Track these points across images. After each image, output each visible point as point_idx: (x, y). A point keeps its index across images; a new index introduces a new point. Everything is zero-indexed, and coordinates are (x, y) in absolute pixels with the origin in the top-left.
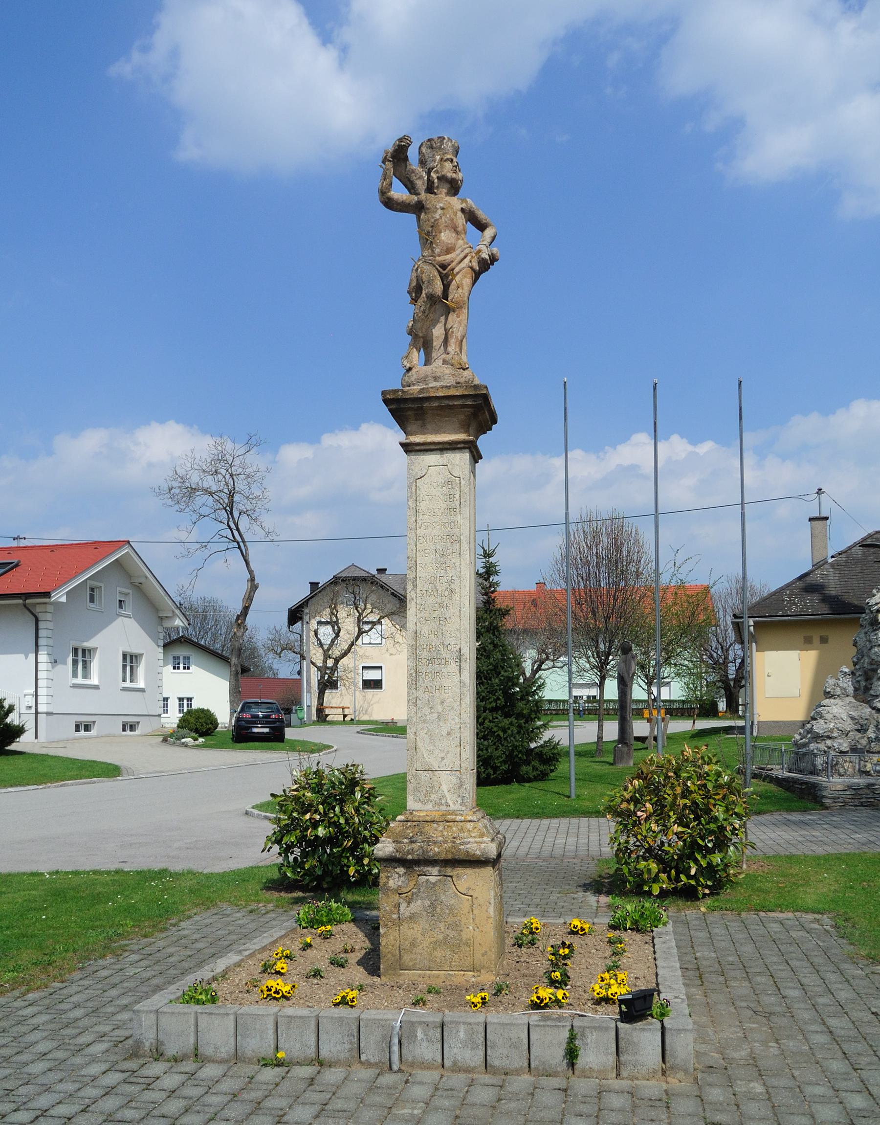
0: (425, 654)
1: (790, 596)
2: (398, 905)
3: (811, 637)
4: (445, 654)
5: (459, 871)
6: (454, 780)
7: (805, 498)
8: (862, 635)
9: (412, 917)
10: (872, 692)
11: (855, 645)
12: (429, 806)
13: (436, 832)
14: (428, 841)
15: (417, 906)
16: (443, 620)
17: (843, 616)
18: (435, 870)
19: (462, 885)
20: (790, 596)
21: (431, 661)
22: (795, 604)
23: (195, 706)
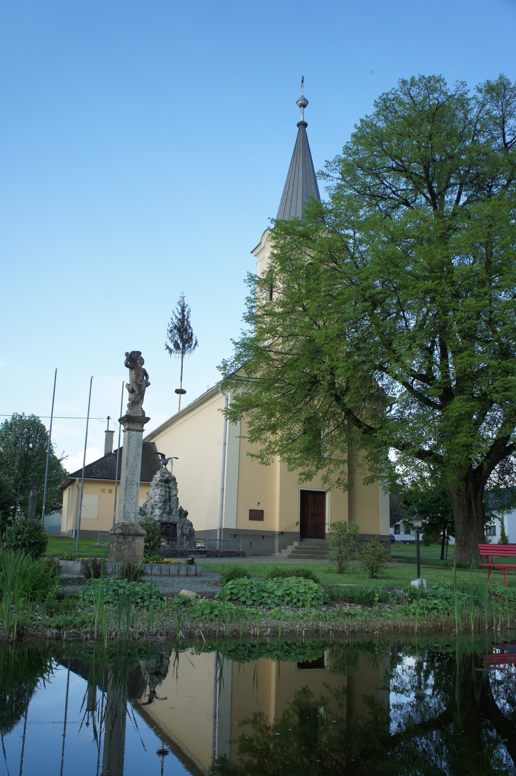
0: (129, 482)
1: (96, 468)
2: (121, 546)
3: (105, 490)
4: (134, 483)
5: (137, 537)
6: (134, 515)
7: (101, 420)
8: (151, 490)
9: (124, 549)
10: (154, 514)
11: (148, 494)
12: (127, 522)
13: (131, 528)
14: (130, 530)
15: (125, 546)
16: (134, 474)
17: (109, 480)
18: (130, 537)
19: (137, 541)
20: (96, 468)
21: (130, 484)
22: (99, 473)
23: (314, 476)
